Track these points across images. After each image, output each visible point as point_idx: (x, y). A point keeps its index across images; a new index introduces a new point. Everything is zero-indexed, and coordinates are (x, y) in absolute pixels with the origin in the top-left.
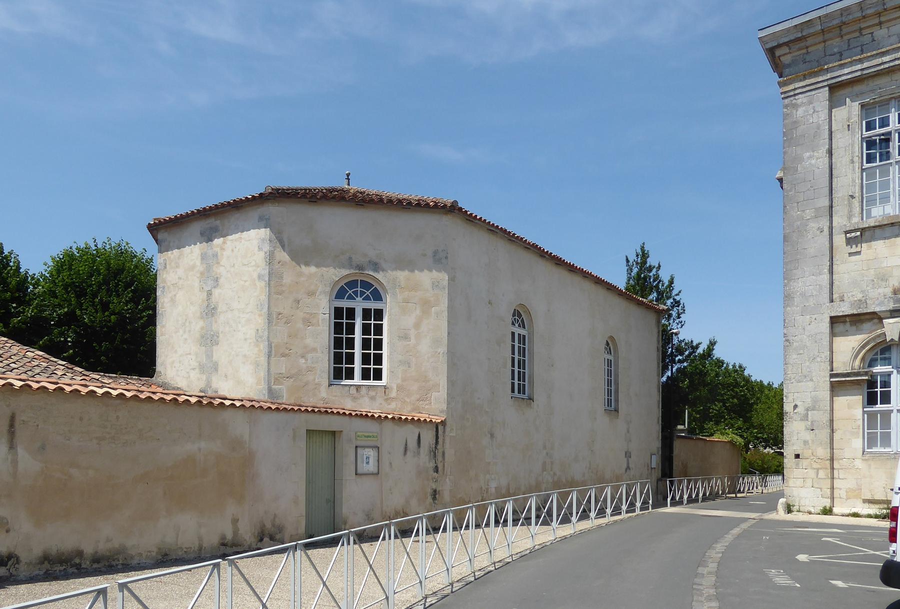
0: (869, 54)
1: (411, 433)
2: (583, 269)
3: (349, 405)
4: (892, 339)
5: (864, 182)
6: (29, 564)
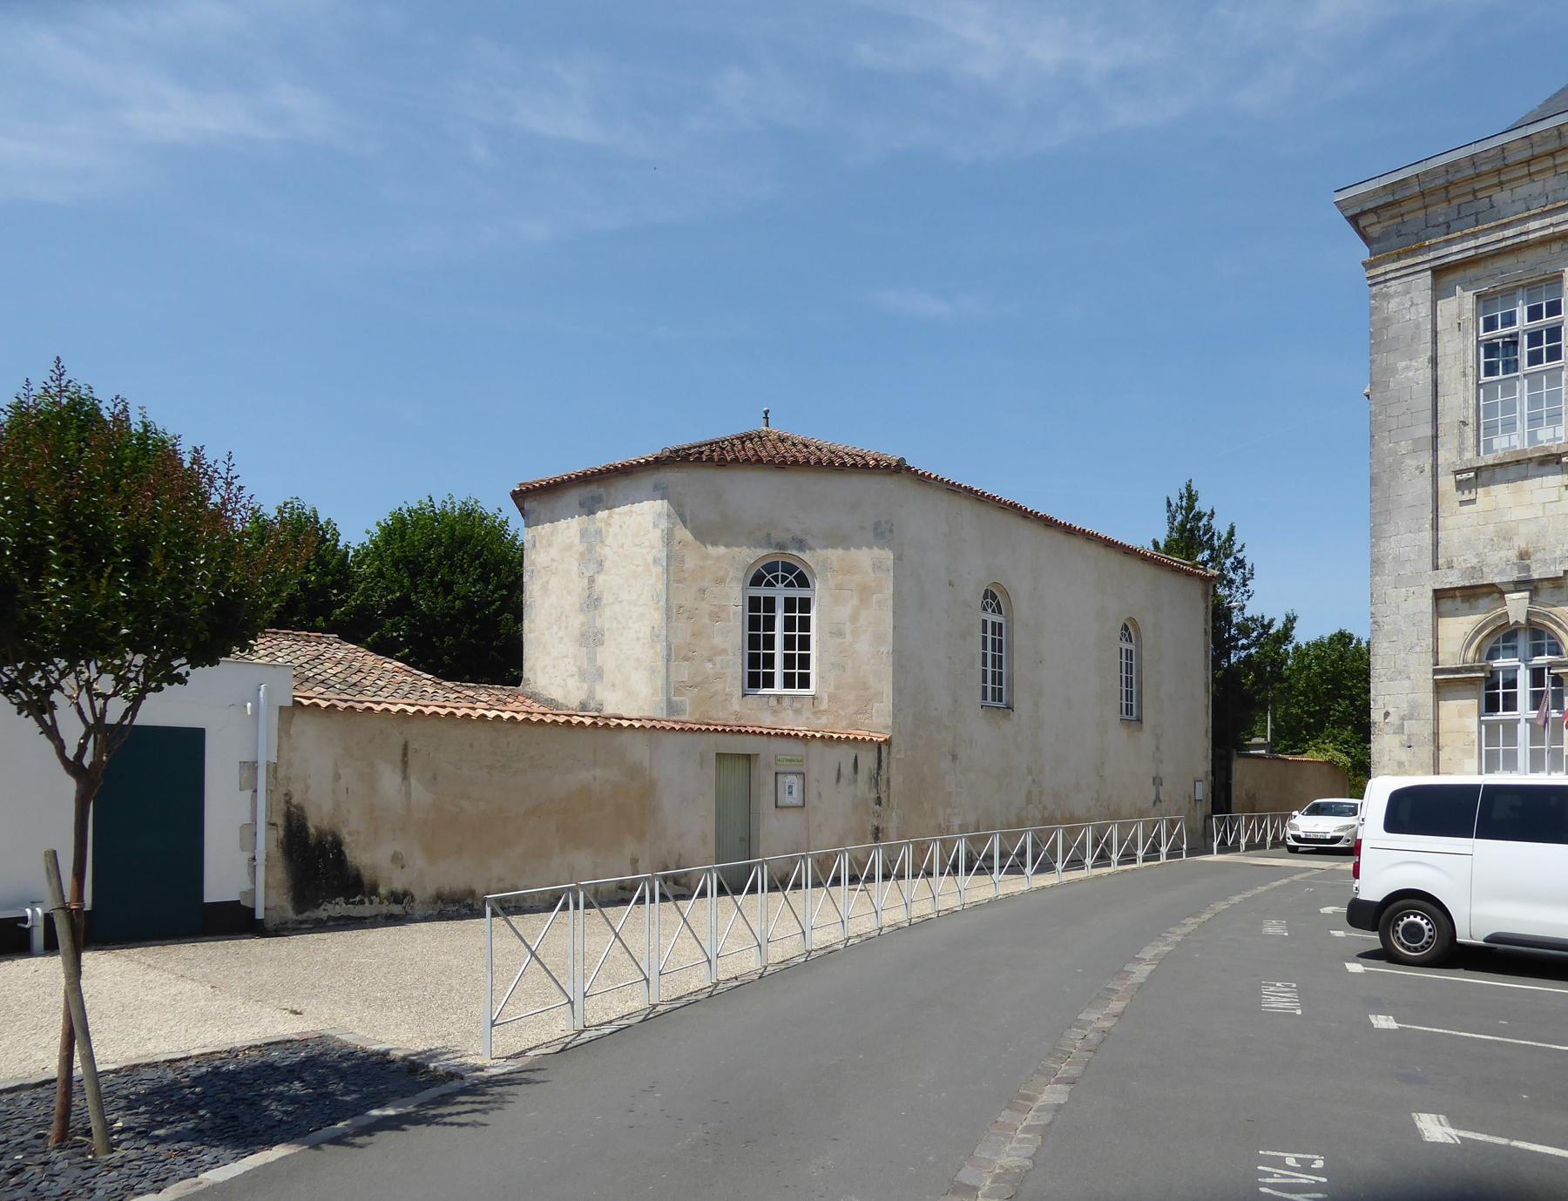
0: (1485, 226)
1: (845, 755)
2: (1084, 530)
3: (767, 721)
4: (1517, 621)
5: (1482, 403)
6: (423, 903)
